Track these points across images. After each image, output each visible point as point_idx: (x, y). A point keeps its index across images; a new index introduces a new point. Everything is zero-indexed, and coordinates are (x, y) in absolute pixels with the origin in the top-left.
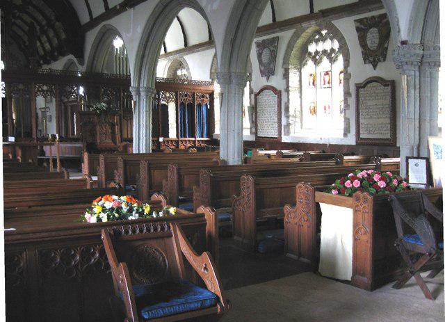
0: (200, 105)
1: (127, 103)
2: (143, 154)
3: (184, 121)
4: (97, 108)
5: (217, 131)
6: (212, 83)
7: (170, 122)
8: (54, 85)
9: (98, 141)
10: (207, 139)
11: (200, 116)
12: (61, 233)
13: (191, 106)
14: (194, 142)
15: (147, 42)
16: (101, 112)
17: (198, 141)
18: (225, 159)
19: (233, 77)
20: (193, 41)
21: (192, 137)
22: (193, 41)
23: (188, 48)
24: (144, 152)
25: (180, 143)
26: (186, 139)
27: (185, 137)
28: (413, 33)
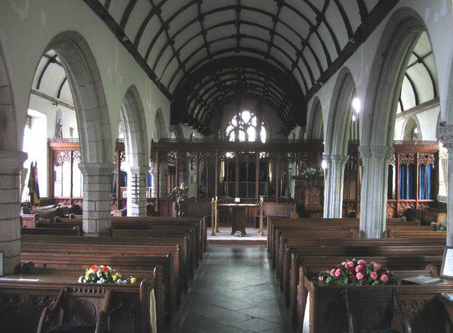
0: (423, 166)
1: (354, 166)
2: (331, 219)
3: (405, 183)
4: (307, 174)
5: (443, 191)
6: (437, 143)
7: (440, 181)
8: (297, 152)
9: (307, 203)
10: (431, 201)
11: (422, 177)
12: (43, 286)
13: (413, 167)
14: (415, 203)
15: (335, 112)
16: (309, 177)
17: (420, 203)
18: (364, 230)
19: (372, 152)
20: (423, 99)
21: (413, 199)
22: (423, 99)
23: (419, 106)
24: (331, 216)
25: (399, 205)
26: (405, 201)
27: (405, 198)
28: (449, 116)
